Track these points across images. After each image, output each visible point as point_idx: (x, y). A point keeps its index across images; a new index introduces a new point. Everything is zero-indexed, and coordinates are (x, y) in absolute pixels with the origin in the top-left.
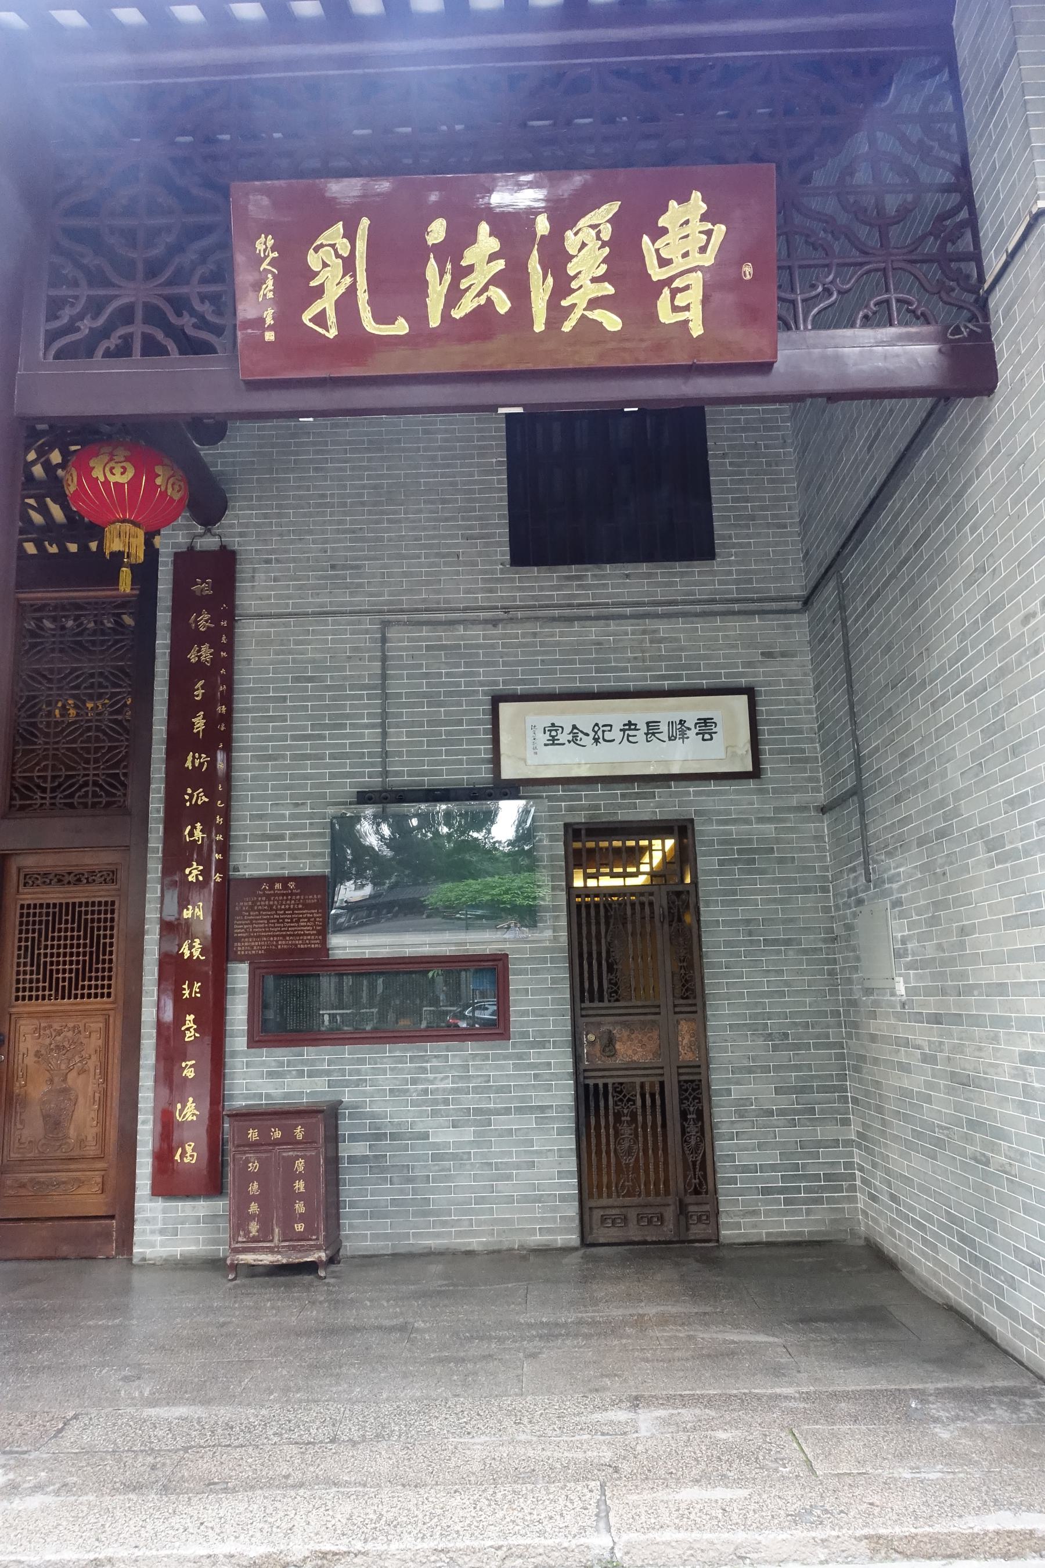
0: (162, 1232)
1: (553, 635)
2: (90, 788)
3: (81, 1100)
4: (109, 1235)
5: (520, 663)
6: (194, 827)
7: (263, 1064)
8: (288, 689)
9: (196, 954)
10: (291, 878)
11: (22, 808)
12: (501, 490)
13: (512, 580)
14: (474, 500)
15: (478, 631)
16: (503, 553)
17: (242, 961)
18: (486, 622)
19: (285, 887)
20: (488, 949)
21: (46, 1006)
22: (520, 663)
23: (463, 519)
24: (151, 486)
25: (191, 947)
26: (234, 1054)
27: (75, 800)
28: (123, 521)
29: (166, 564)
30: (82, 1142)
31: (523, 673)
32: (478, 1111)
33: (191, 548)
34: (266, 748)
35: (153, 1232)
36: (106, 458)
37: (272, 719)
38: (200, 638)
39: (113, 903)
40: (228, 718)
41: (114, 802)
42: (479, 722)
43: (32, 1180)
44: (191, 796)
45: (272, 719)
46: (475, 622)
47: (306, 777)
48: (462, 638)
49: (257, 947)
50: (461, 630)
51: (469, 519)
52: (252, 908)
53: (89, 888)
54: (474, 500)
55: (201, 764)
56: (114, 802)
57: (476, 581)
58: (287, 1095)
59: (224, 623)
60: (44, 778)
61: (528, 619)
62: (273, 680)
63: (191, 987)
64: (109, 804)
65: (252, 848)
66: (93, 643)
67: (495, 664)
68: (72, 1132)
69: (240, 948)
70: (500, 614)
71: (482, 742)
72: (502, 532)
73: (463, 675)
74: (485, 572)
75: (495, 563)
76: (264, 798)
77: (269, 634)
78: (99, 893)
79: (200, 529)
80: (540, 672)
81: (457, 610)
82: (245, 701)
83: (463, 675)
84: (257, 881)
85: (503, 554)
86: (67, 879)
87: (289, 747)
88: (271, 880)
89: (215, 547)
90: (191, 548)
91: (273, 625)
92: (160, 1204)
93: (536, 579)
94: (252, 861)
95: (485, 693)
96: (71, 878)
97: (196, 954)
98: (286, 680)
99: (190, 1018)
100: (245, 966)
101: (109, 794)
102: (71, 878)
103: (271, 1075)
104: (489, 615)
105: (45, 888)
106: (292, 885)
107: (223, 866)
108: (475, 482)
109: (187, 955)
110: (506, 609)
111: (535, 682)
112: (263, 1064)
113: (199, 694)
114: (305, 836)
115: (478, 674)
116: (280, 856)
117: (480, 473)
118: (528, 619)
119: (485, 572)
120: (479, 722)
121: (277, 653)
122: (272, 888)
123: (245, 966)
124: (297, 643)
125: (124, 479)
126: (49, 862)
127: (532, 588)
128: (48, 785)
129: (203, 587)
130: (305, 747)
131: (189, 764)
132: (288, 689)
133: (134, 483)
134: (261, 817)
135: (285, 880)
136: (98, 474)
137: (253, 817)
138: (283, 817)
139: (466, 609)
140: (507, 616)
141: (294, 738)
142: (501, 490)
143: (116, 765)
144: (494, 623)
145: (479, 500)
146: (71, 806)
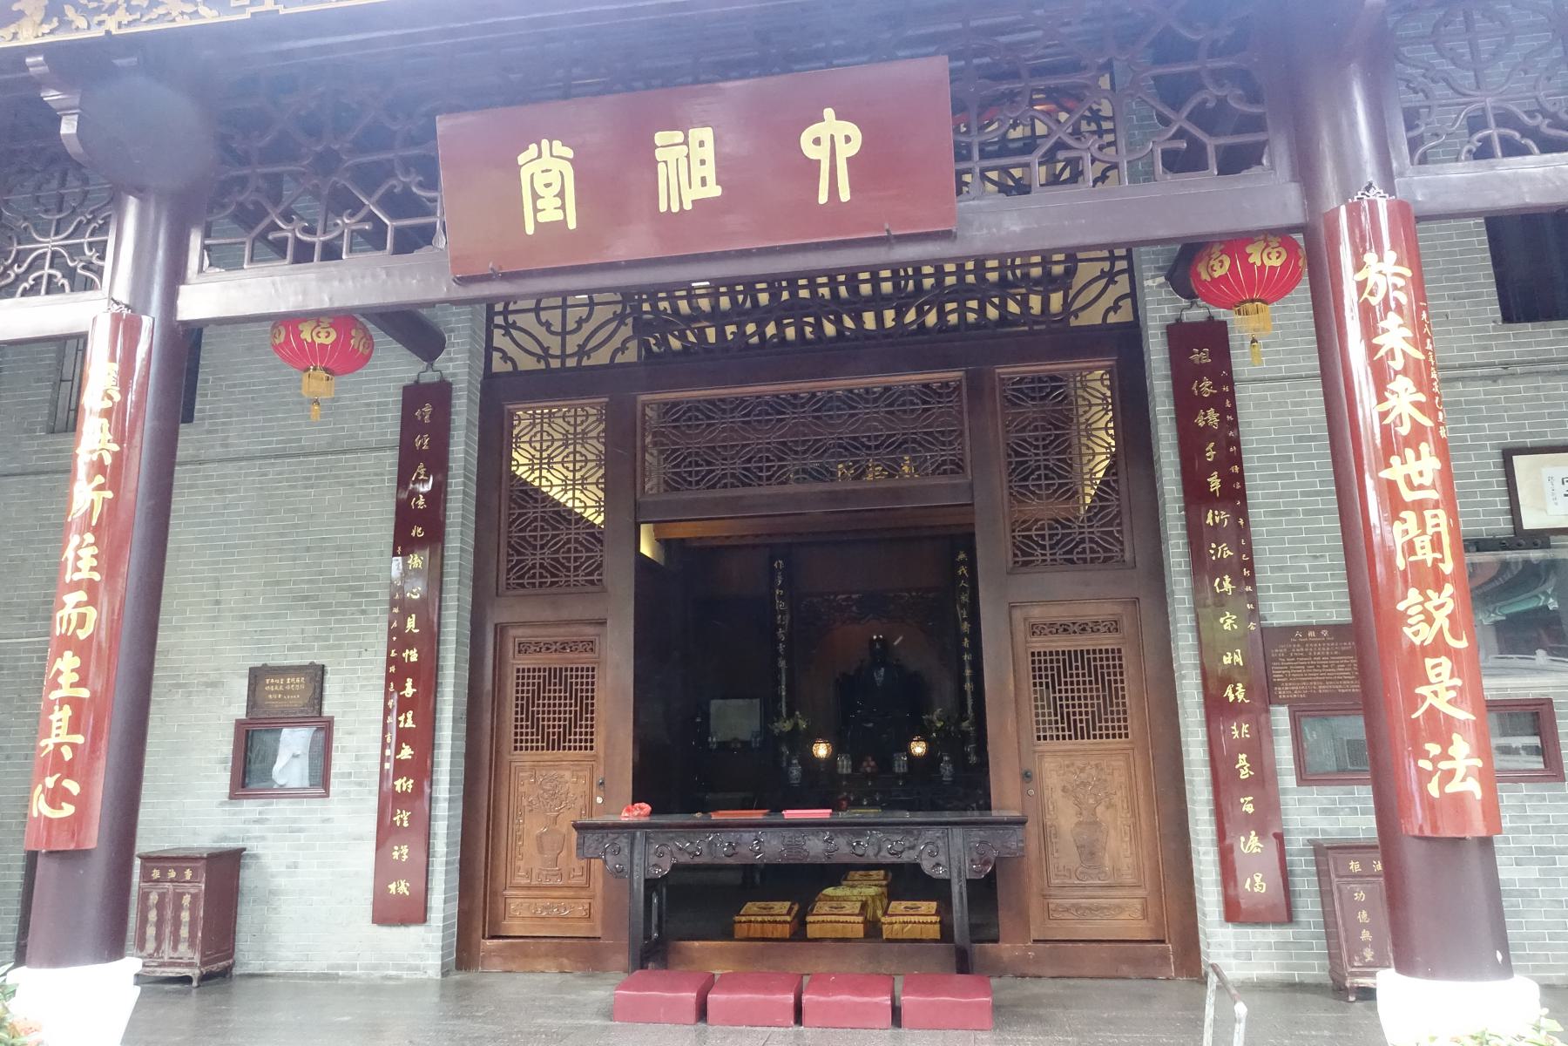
0: (1236, 956)
1: (1557, 389)
2: (1087, 545)
3: (1112, 833)
4: (1164, 958)
5: (1525, 417)
6: (1222, 580)
7: (1315, 801)
8: (1292, 449)
9: (1241, 697)
10: (1325, 627)
11: (1025, 564)
12: (1483, 251)
13: (1507, 337)
14: (1456, 262)
15: (1478, 389)
16: (1494, 310)
17: (1281, 703)
18: (1484, 378)
19: (1319, 635)
20: (1532, 694)
21: (1068, 745)
22: (1525, 417)
23: (1447, 280)
24: (1249, 268)
25: (1234, 691)
26: (1286, 791)
27: (1075, 557)
28: (1253, 301)
29: (1155, 336)
30: (1116, 870)
31: (1531, 426)
32: (1540, 850)
33: (1179, 320)
34: (1277, 505)
35: (1227, 956)
36: (1263, 245)
37: (1279, 477)
38: (1206, 404)
39: (1119, 651)
40: (1240, 477)
41: (1111, 558)
42: (1492, 475)
43: (1073, 905)
44: (1216, 550)
45: (1279, 477)
46: (1474, 378)
47: (1321, 531)
48: (1461, 394)
49: (1297, 691)
50: (1460, 386)
51: (1454, 280)
52: (1287, 655)
53: (1095, 636)
54: (1456, 262)
55: (1222, 521)
56: (1111, 558)
57: (1469, 339)
58: (1342, 831)
59: (1226, 389)
60: (1043, 537)
61: (1530, 373)
62: (1275, 441)
63: (1239, 728)
64: (1106, 560)
65: (1276, 598)
66: (839, 408)
67: (1500, 418)
68: (1107, 862)
69: (1281, 692)
70: (1499, 370)
71: (1497, 494)
72: (1490, 291)
73: (1468, 430)
74: (1478, 330)
75: (1486, 321)
76: (1282, 551)
77: (1265, 398)
78: (1106, 641)
79: (1184, 302)
80: (1550, 425)
81: (1454, 368)
82: (1250, 460)
83: (1468, 430)
84: (1289, 630)
85: (1493, 311)
86: (1072, 628)
87: (1300, 503)
88: (1304, 629)
89: (1202, 319)
90: (1179, 320)
91: (1269, 389)
92: (1230, 930)
93: (1531, 335)
94: (1279, 611)
95: (1493, 447)
96: (1076, 628)
97: (1241, 697)
98: (1288, 440)
99: (1242, 757)
100: (1284, 709)
101: (1106, 550)
102: (1076, 628)
103: (1324, 811)
104: (1486, 371)
105: (1055, 637)
106: (1325, 633)
107: (1254, 614)
108: (1452, 245)
109: (1231, 698)
110: (1506, 365)
111: (1544, 434)
112: (1315, 801)
113: (1210, 455)
114: (1328, 586)
115: (1484, 429)
116: (1306, 606)
117: (1458, 236)
118: (1530, 373)
119: (1478, 330)
120: (1492, 475)
121: (1275, 415)
122: (1305, 635)
123: (1284, 709)
124: (1295, 404)
125: (1277, 263)
126: (1057, 613)
127: (1529, 345)
128: (1047, 543)
129: (1201, 357)
130: (1316, 503)
131: (1210, 521)
132: (1292, 449)
133: (1284, 266)
134: (1281, 569)
135: (1318, 628)
136: (1255, 259)
137: (1273, 570)
138: (1303, 568)
139: (1462, 367)
140: (1505, 371)
141: (1304, 494)
142: (1483, 251)
143: (1110, 523)
144: (1494, 379)
145: (1462, 261)
146: (1071, 561)
